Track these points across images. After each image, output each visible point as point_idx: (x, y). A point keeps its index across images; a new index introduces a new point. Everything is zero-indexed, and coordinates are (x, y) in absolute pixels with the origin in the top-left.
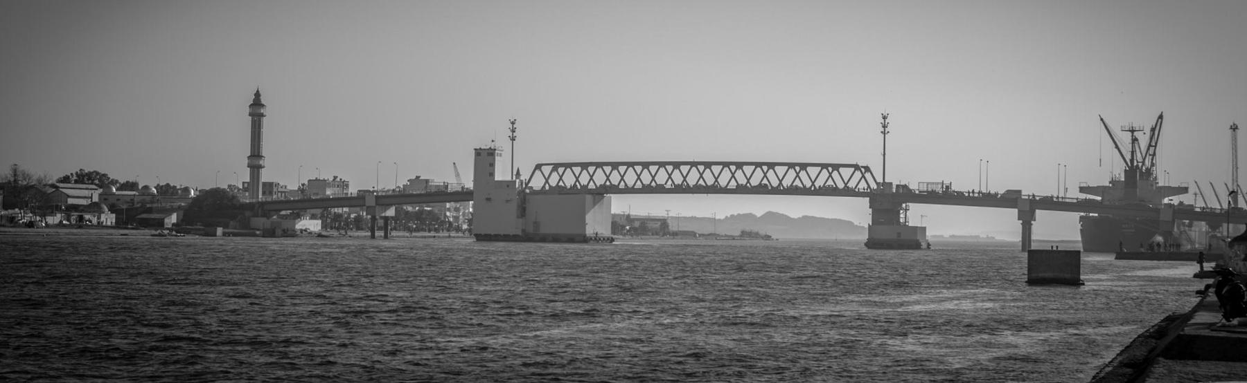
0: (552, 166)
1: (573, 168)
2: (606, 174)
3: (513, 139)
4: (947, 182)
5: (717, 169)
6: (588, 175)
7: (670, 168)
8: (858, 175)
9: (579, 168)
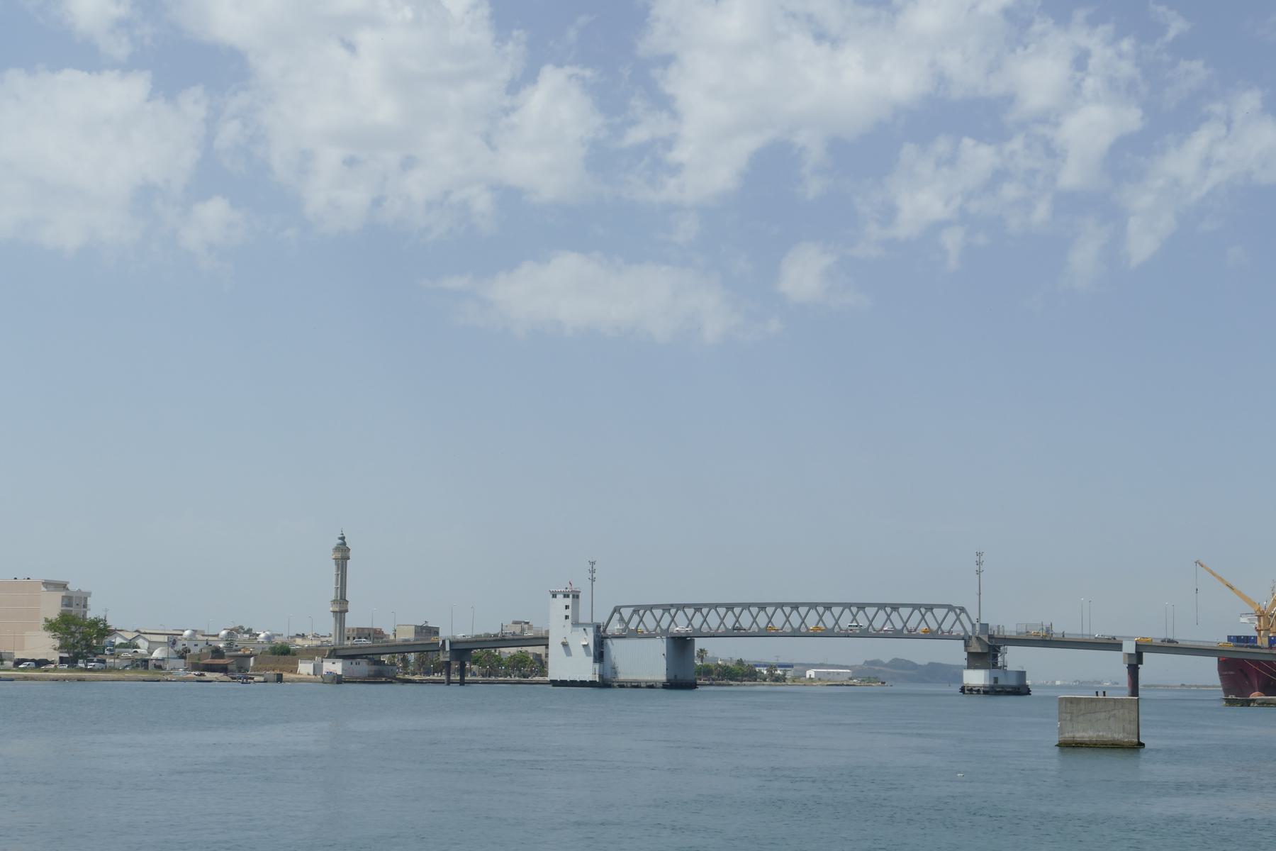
0: (632, 609)
1: (784, 608)
2: (786, 615)
3: (593, 580)
6: (685, 618)
7: (754, 610)
8: (952, 616)
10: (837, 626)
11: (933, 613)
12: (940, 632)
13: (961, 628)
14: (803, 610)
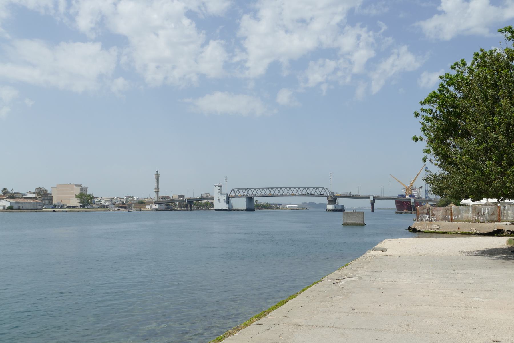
4: (349, 192)
5: (252, 190)
9: (253, 190)
14: (292, 189)
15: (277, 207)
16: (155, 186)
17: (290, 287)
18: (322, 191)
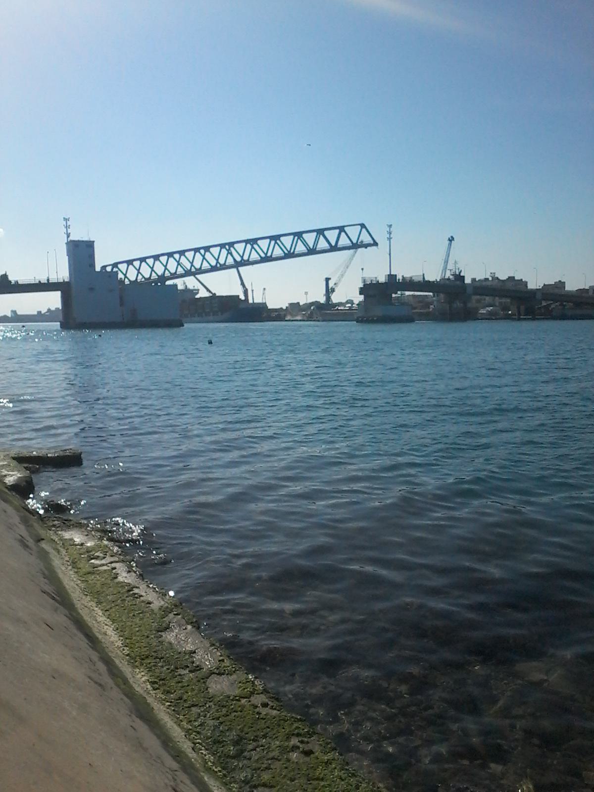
6: (175, 261)
9: (166, 257)
10: (193, 267)
11: (168, 259)
12: (218, 265)
13: (182, 270)
14: (164, 259)
15: (233, 407)
16: (239, 282)
17: (184, 466)
18: (348, 237)
